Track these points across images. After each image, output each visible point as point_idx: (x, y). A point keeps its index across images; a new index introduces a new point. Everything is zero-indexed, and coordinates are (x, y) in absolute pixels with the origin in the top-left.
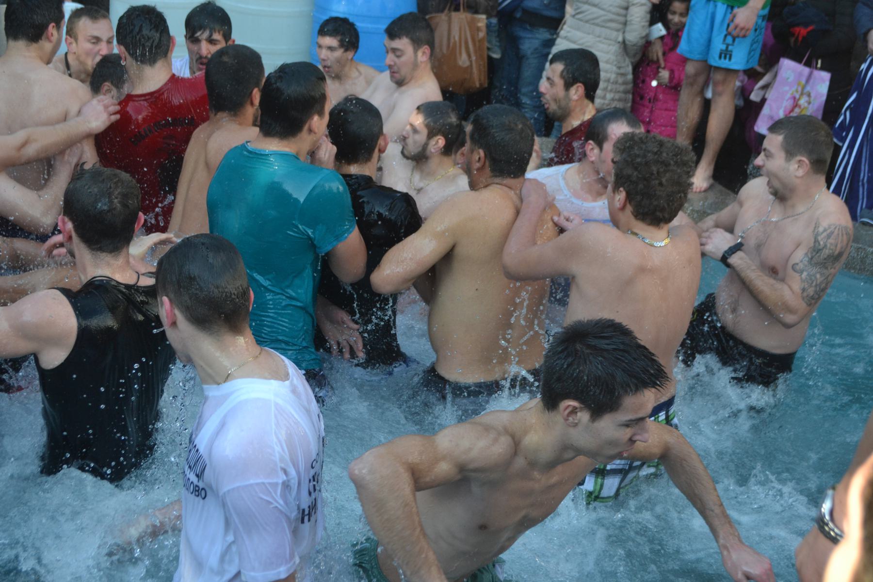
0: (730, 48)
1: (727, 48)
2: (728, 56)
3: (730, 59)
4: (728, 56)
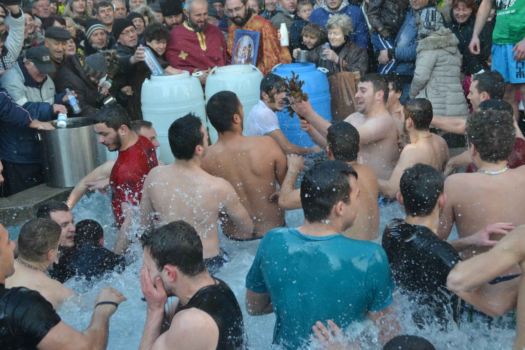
0: (522, 70)
1: (520, 70)
2: (522, 75)
3: (524, 77)
4: (522, 75)
